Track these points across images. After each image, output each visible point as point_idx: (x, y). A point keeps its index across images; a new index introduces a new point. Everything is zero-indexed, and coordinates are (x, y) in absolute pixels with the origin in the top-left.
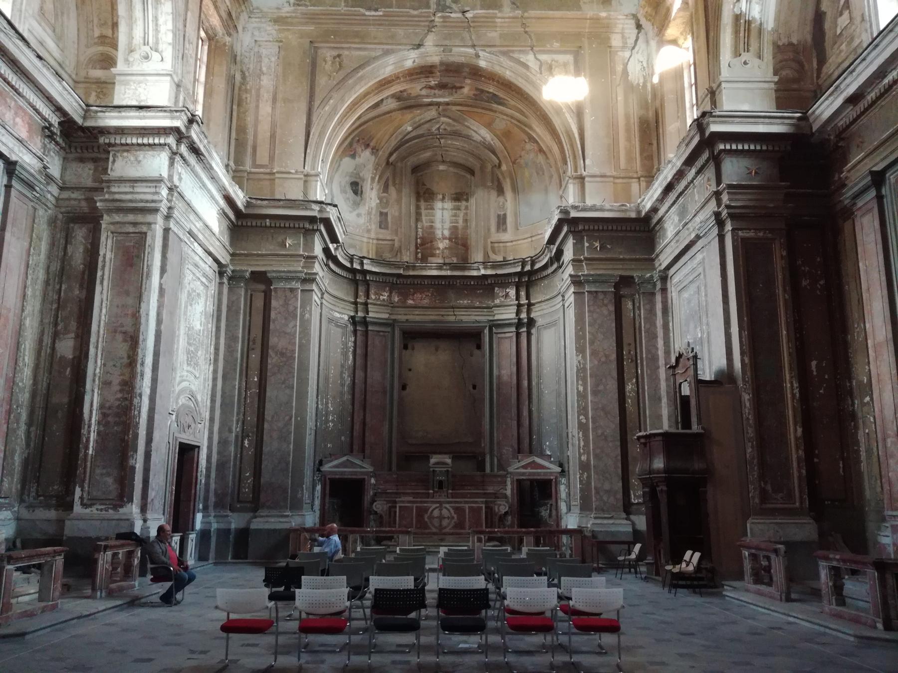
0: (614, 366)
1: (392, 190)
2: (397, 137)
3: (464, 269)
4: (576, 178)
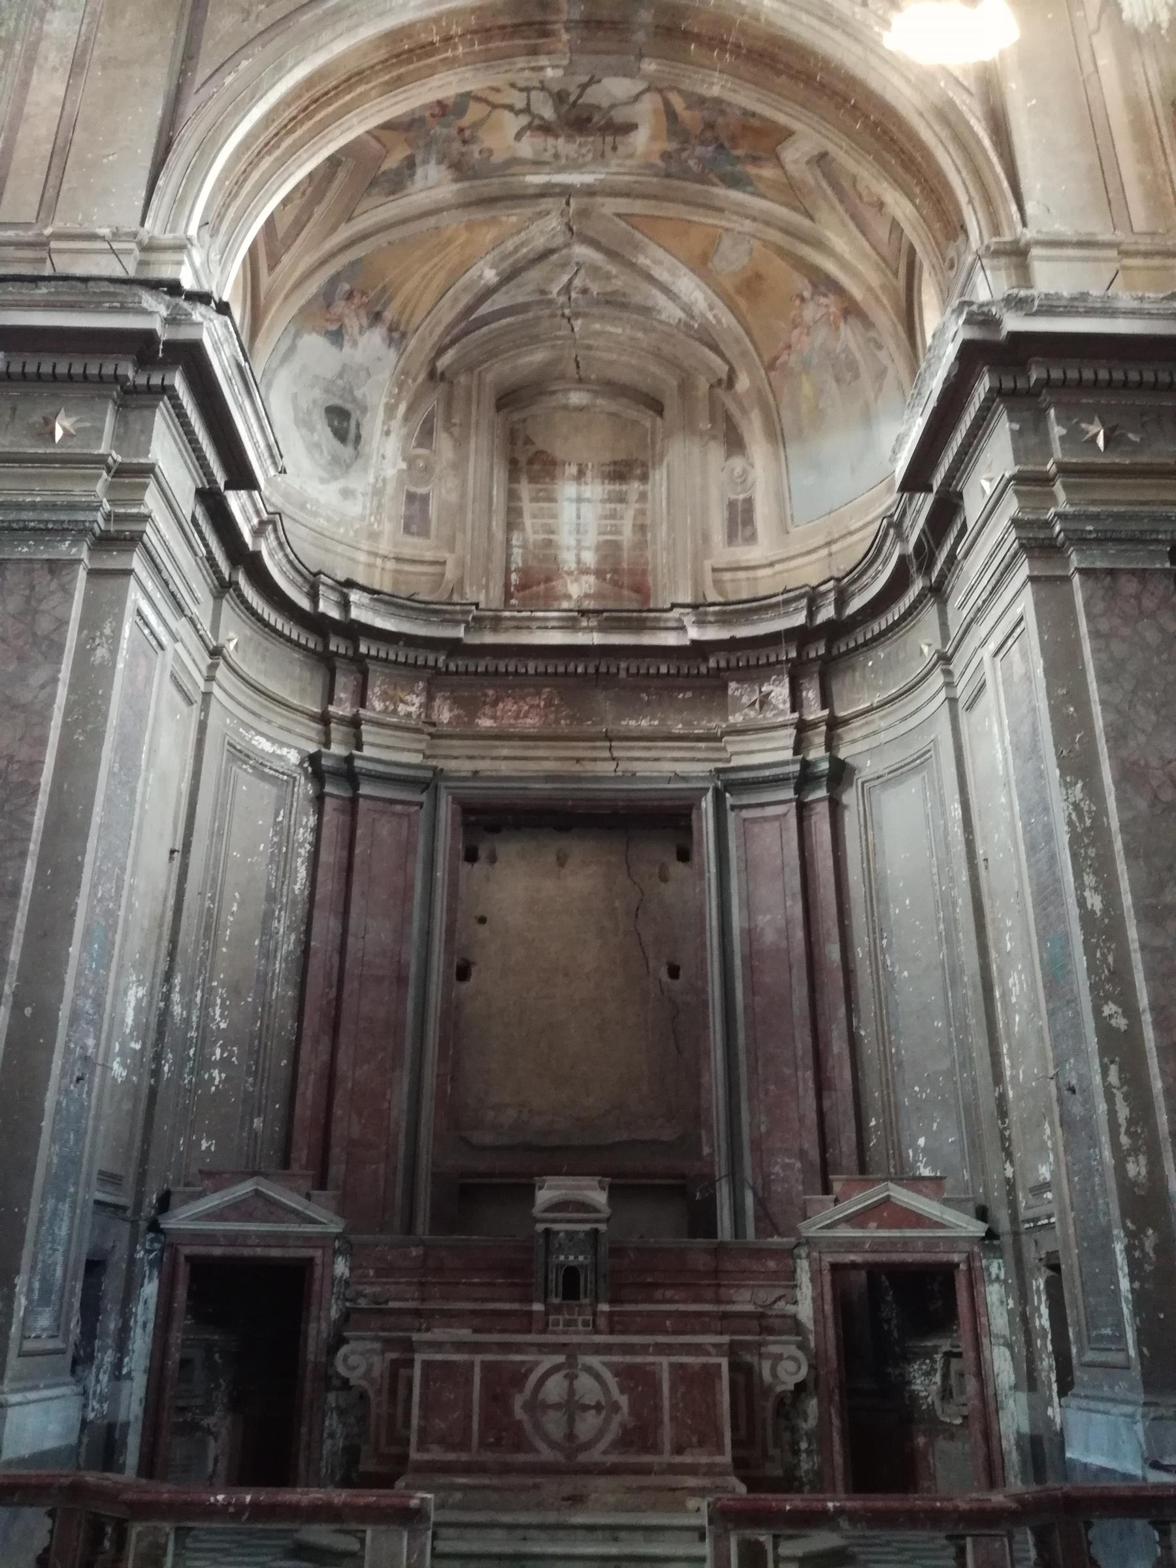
1: (444, 443)
2: (456, 300)
3: (640, 625)
4: (996, 254)
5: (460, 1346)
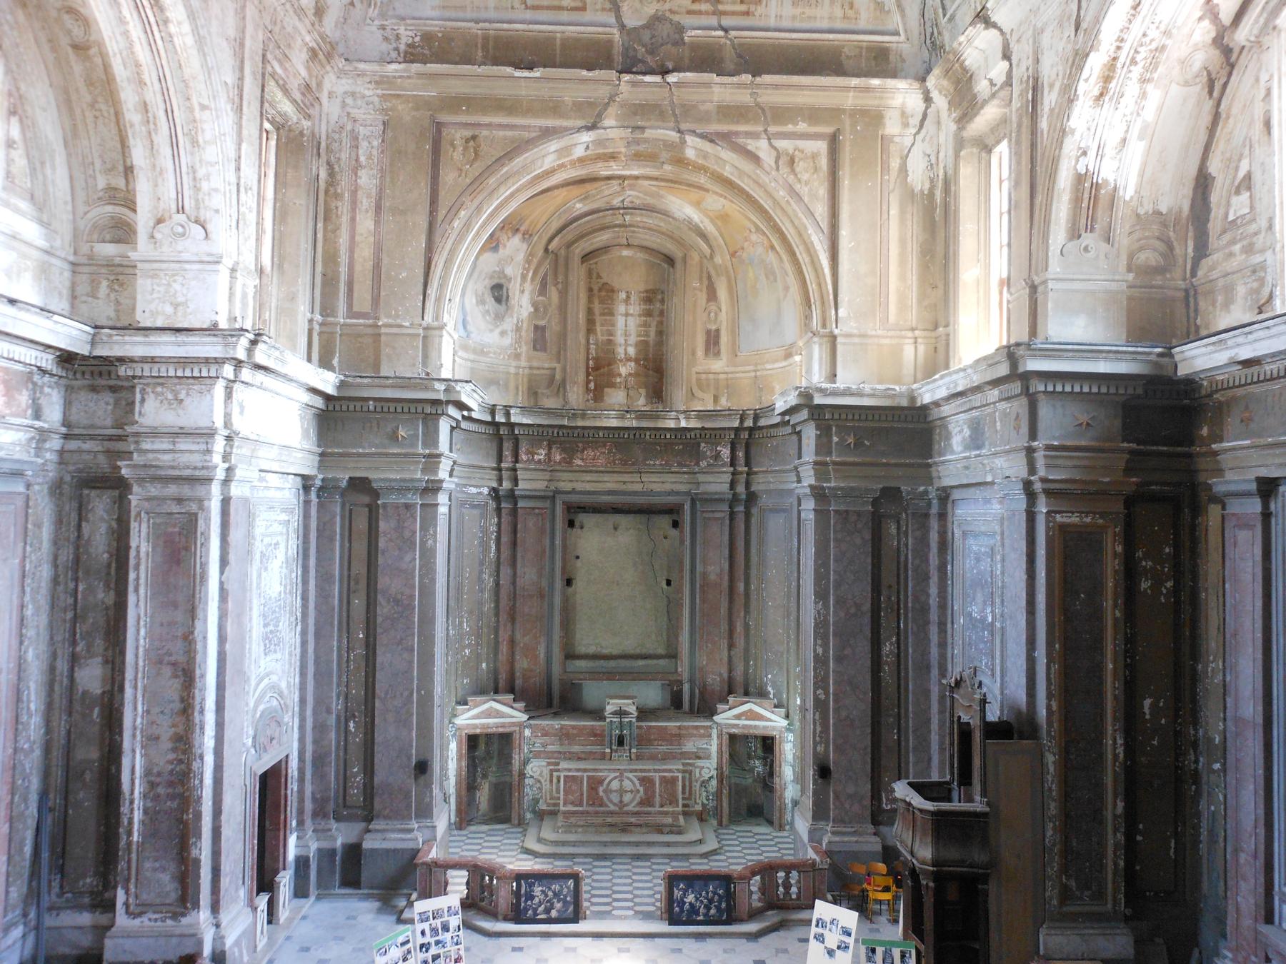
0: (867, 620)
5: (578, 770)
